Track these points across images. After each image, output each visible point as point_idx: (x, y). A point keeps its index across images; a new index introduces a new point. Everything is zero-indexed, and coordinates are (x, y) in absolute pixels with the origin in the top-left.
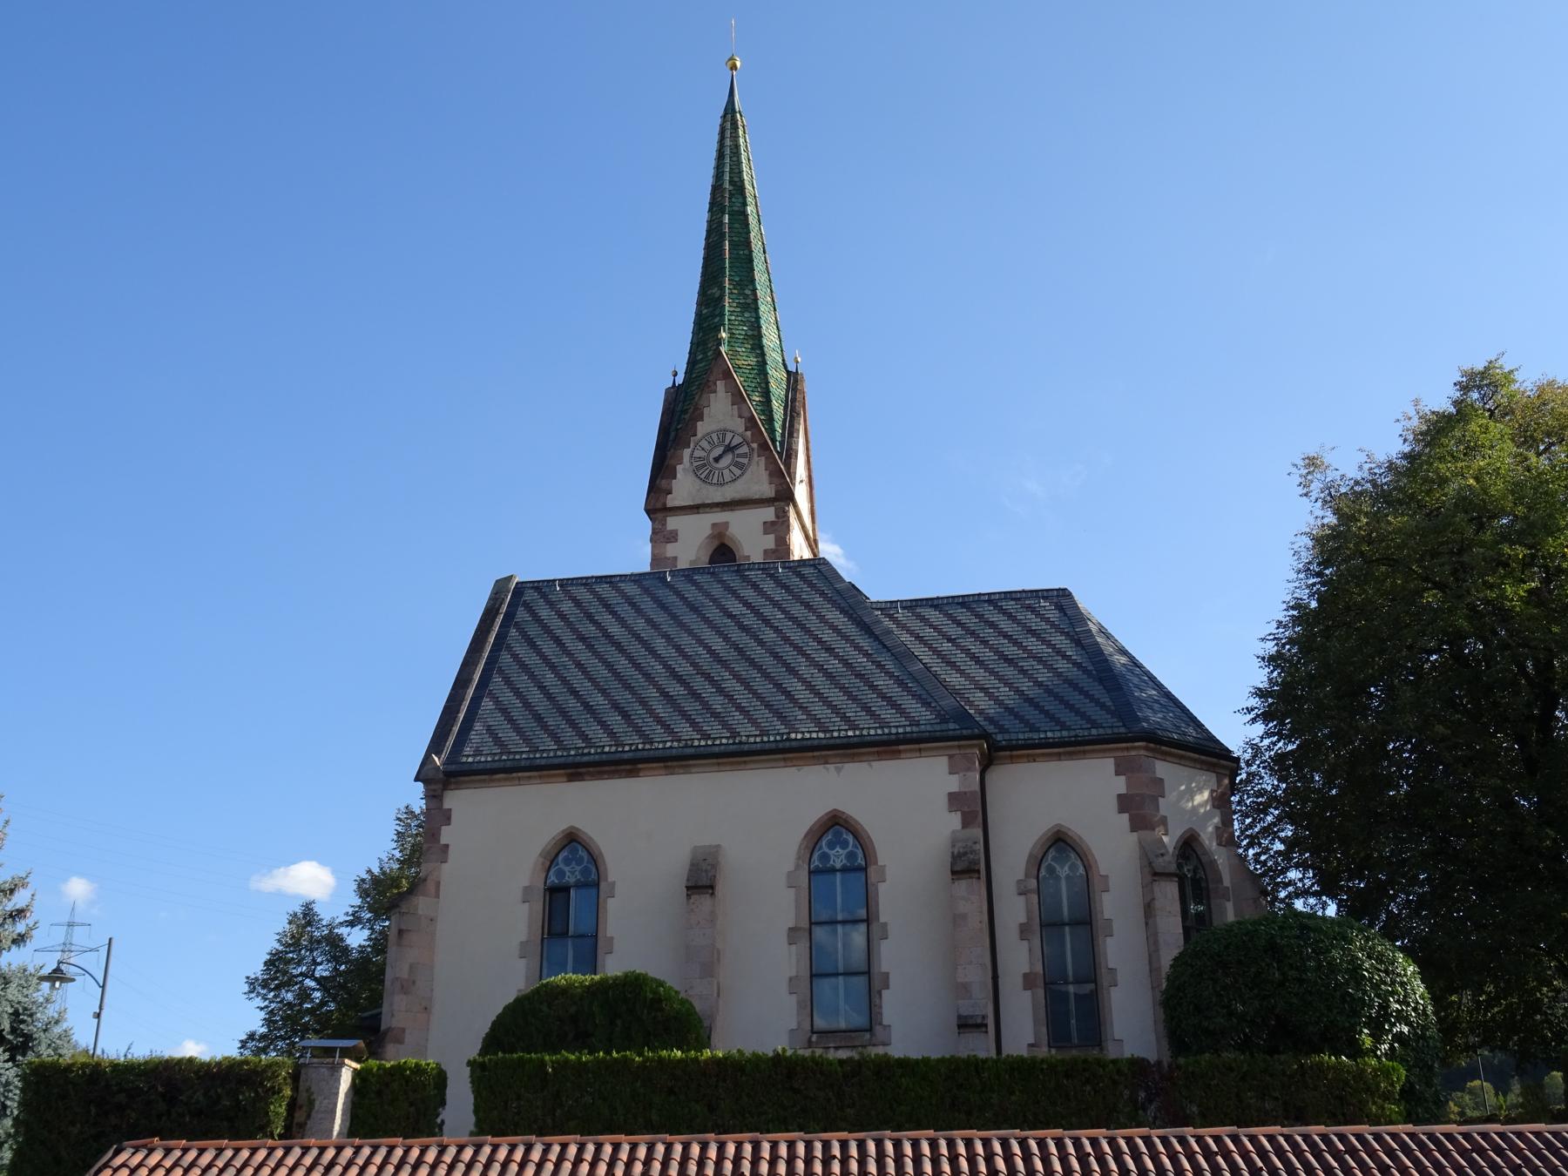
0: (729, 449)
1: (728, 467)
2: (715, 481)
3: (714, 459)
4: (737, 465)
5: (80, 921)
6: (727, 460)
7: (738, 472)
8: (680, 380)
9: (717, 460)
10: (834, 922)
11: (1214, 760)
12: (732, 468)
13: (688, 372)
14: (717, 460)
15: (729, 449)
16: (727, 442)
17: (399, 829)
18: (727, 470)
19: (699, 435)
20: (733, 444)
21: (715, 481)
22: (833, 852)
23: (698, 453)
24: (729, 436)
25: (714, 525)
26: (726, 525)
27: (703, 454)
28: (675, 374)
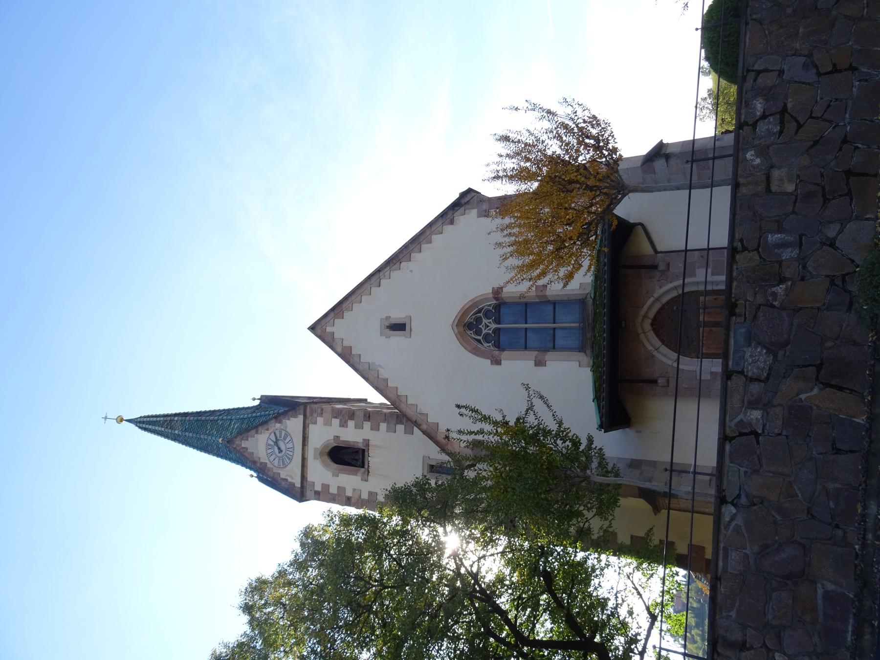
0: (276, 443)
1: (285, 445)
2: (291, 454)
3: (279, 453)
4: (285, 439)
5: (699, 471)
6: (281, 444)
7: (288, 439)
8: (255, 475)
9: (280, 451)
10: (693, 500)
11: (721, 552)
12: (286, 442)
13: (251, 469)
14: (280, 451)
15: (276, 443)
16: (273, 444)
17: (764, 98)
18: (287, 445)
19: (267, 461)
20: (275, 440)
21: (291, 454)
22: (483, 329)
23: (276, 463)
24: (270, 442)
25: (315, 458)
26: (316, 449)
27: (277, 460)
28: (252, 476)
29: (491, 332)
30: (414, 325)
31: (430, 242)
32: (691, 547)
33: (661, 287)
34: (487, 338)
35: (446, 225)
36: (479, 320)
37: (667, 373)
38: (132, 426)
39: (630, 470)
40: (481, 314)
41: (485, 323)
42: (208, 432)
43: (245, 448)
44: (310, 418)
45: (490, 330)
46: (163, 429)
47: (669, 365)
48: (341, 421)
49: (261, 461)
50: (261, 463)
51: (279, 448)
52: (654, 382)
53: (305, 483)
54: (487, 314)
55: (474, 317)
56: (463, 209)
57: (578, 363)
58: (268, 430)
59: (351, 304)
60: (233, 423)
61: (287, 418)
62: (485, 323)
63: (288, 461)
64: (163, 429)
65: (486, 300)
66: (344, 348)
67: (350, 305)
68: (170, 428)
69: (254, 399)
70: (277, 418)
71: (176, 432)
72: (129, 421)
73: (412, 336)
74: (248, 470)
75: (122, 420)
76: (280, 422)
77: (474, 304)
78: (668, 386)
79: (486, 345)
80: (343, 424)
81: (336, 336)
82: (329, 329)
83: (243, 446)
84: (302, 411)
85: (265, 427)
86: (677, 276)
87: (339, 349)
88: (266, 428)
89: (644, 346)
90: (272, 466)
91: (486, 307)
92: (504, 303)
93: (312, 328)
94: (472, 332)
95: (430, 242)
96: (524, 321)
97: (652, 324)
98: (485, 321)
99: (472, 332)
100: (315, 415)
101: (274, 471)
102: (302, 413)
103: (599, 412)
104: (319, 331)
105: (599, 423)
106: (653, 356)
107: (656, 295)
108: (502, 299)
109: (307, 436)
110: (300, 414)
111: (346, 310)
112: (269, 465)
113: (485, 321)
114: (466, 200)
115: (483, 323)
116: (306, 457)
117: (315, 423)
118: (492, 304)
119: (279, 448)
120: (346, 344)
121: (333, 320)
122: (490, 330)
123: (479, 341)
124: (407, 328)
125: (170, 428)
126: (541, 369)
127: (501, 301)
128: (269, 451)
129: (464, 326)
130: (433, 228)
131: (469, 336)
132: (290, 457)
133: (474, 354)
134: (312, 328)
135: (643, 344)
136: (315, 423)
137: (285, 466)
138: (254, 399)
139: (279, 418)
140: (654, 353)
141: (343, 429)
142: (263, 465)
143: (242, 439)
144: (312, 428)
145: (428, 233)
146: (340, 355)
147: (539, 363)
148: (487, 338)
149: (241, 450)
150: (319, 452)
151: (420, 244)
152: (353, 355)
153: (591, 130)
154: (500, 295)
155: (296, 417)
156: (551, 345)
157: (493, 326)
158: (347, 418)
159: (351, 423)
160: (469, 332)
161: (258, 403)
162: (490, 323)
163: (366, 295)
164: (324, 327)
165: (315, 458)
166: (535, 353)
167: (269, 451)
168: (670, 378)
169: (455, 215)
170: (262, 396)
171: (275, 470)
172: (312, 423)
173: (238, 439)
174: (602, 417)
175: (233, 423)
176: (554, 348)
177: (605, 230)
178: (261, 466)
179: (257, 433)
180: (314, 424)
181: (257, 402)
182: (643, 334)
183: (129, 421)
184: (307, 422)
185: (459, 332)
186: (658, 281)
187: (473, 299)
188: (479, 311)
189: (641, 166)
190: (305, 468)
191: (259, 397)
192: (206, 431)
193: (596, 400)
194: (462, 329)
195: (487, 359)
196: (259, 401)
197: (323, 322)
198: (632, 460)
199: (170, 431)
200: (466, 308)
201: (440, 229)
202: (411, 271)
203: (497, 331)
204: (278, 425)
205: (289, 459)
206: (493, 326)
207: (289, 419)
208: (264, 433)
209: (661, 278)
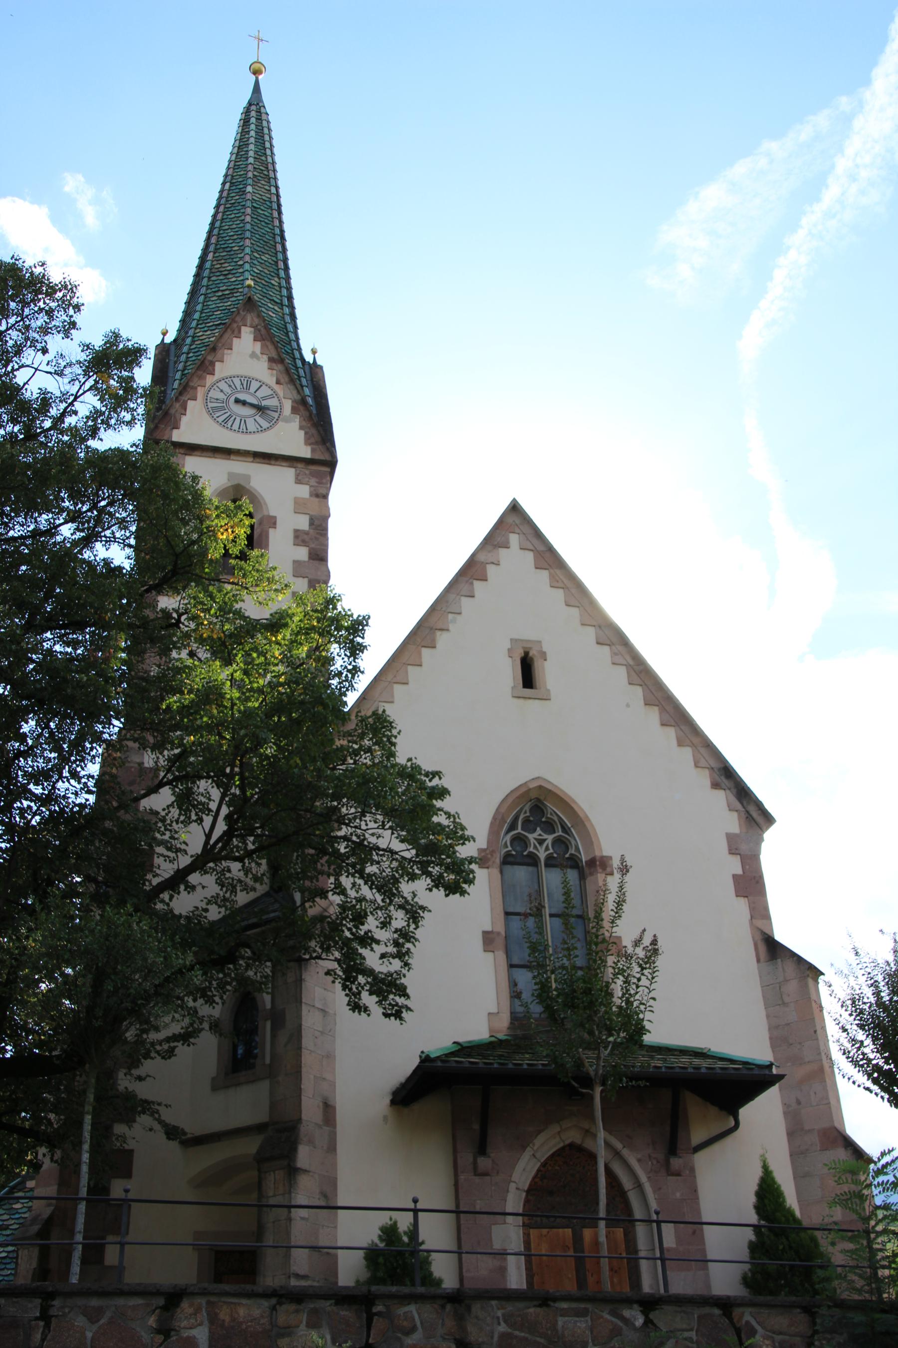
2: (236, 426)
21: (236, 426)
22: (535, 835)
25: (231, 475)
27: (221, 396)
29: (531, 849)
30: (533, 705)
31: (680, 744)
32: (125, 1203)
33: (639, 1160)
34: (519, 840)
35: (710, 775)
36: (549, 827)
37: (498, 1173)
38: (247, 95)
39: (321, 1104)
40: (560, 833)
41: (545, 840)
42: (256, 254)
43: (240, 332)
44: (307, 472)
45: (535, 847)
46: (251, 160)
47: (511, 1176)
48: (306, 533)
49: (218, 364)
50: (212, 364)
51: (244, 403)
52: (482, 1149)
53: (182, 451)
54: (561, 843)
55: (556, 819)
56: (738, 806)
57: (495, 1011)
58: (278, 382)
59: (562, 585)
60: (276, 308)
61: (304, 423)
62: (545, 840)
63: (220, 419)
64: (251, 160)
65: (601, 849)
66: (484, 565)
67: (560, 585)
68: (255, 176)
69: (314, 352)
70: (300, 405)
71: (249, 189)
72: (257, 89)
73: (516, 700)
74: (177, 325)
75: (256, 73)
76: (294, 410)
77: (580, 821)
78: (475, 1175)
79: (508, 838)
80: (299, 538)
81: (502, 552)
82: (514, 539)
83: (243, 329)
84: (318, 456)
85: (284, 378)
86: (660, 1189)
87: (481, 557)
88: (282, 381)
89: (539, 1132)
90: (208, 384)
91: (573, 842)
92: (582, 877)
93: (515, 508)
94: (528, 814)
95: (680, 744)
96: (554, 911)
97: (571, 1146)
98: (550, 838)
99: (528, 814)
100: (313, 481)
101: (199, 388)
102: (317, 457)
103: (446, 1055)
104: (513, 519)
105: (433, 1056)
106: (524, 1148)
107: (625, 1152)
108: (591, 874)
109: (273, 462)
110: (313, 451)
111: (550, 574)
112: (210, 380)
113: (550, 838)
114: (755, 814)
115: (545, 836)
116: (232, 457)
117: (298, 481)
118: (580, 854)
119: (244, 403)
120: (491, 570)
121: (532, 548)
122: (535, 847)
123: (513, 827)
124: (528, 692)
125: (255, 176)
126: (478, 942)
127: (587, 870)
128: (237, 382)
129: (538, 800)
130: (703, 750)
131: (521, 809)
132: (230, 423)
133: (494, 818)
134: (515, 508)
135: (542, 1131)
136: (298, 481)
137: (211, 412)
138: (314, 352)
139: (301, 408)
140: (528, 1149)
141: (291, 536)
142: (210, 368)
143: (255, 327)
144: (288, 473)
145: (696, 740)
146: (473, 556)
147: (488, 939)
148: (519, 840)
149: (235, 325)
150: (243, 483)
151: (676, 725)
152: (472, 584)
153: (164, 837)
154: (600, 870)
155: (307, 442)
156: (516, 961)
157: (542, 855)
158: (313, 546)
159: (302, 553)
160: (527, 808)
161: (307, 360)
162: (547, 849)
163: (581, 615)
164: (517, 530)
165: (231, 475)
166: (500, 928)
167: (237, 382)
168: (488, 1178)
169: (728, 791)
170: (321, 368)
171: (200, 392)
172: (297, 476)
173: (256, 321)
174: (443, 1061)
175: (276, 308)
176: (511, 966)
177: (752, 1069)
178: (207, 363)
179: (271, 360)
180: (296, 478)
181: (309, 358)
182: (558, 1129)
183: (257, 89)
184: (300, 465)
185: (530, 790)
186: (650, 1156)
187: (589, 820)
188: (565, 829)
189: (835, 1128)
190: (210, 454)
191: (319, 363)
192: (257, 251)
193: (457, 1048)
194: (533, 795)
195: (488, 842)
196: (311, 362)
197: (526, 529)
198: (334, 1108)
199: (250, 175)
200: (573, 805)
201: (703, 763)
202: (628, 705)
203: (532, 860)
204: (288, 405)
205: (226, 421)
206: (542, 855)
207: (301, 428)
208: (272, 375)
209: (655, 1162)
